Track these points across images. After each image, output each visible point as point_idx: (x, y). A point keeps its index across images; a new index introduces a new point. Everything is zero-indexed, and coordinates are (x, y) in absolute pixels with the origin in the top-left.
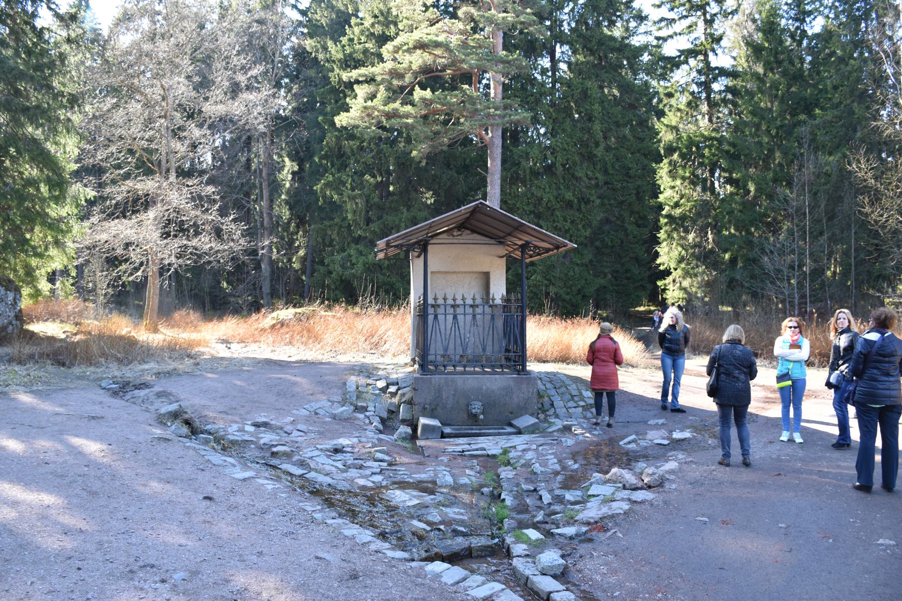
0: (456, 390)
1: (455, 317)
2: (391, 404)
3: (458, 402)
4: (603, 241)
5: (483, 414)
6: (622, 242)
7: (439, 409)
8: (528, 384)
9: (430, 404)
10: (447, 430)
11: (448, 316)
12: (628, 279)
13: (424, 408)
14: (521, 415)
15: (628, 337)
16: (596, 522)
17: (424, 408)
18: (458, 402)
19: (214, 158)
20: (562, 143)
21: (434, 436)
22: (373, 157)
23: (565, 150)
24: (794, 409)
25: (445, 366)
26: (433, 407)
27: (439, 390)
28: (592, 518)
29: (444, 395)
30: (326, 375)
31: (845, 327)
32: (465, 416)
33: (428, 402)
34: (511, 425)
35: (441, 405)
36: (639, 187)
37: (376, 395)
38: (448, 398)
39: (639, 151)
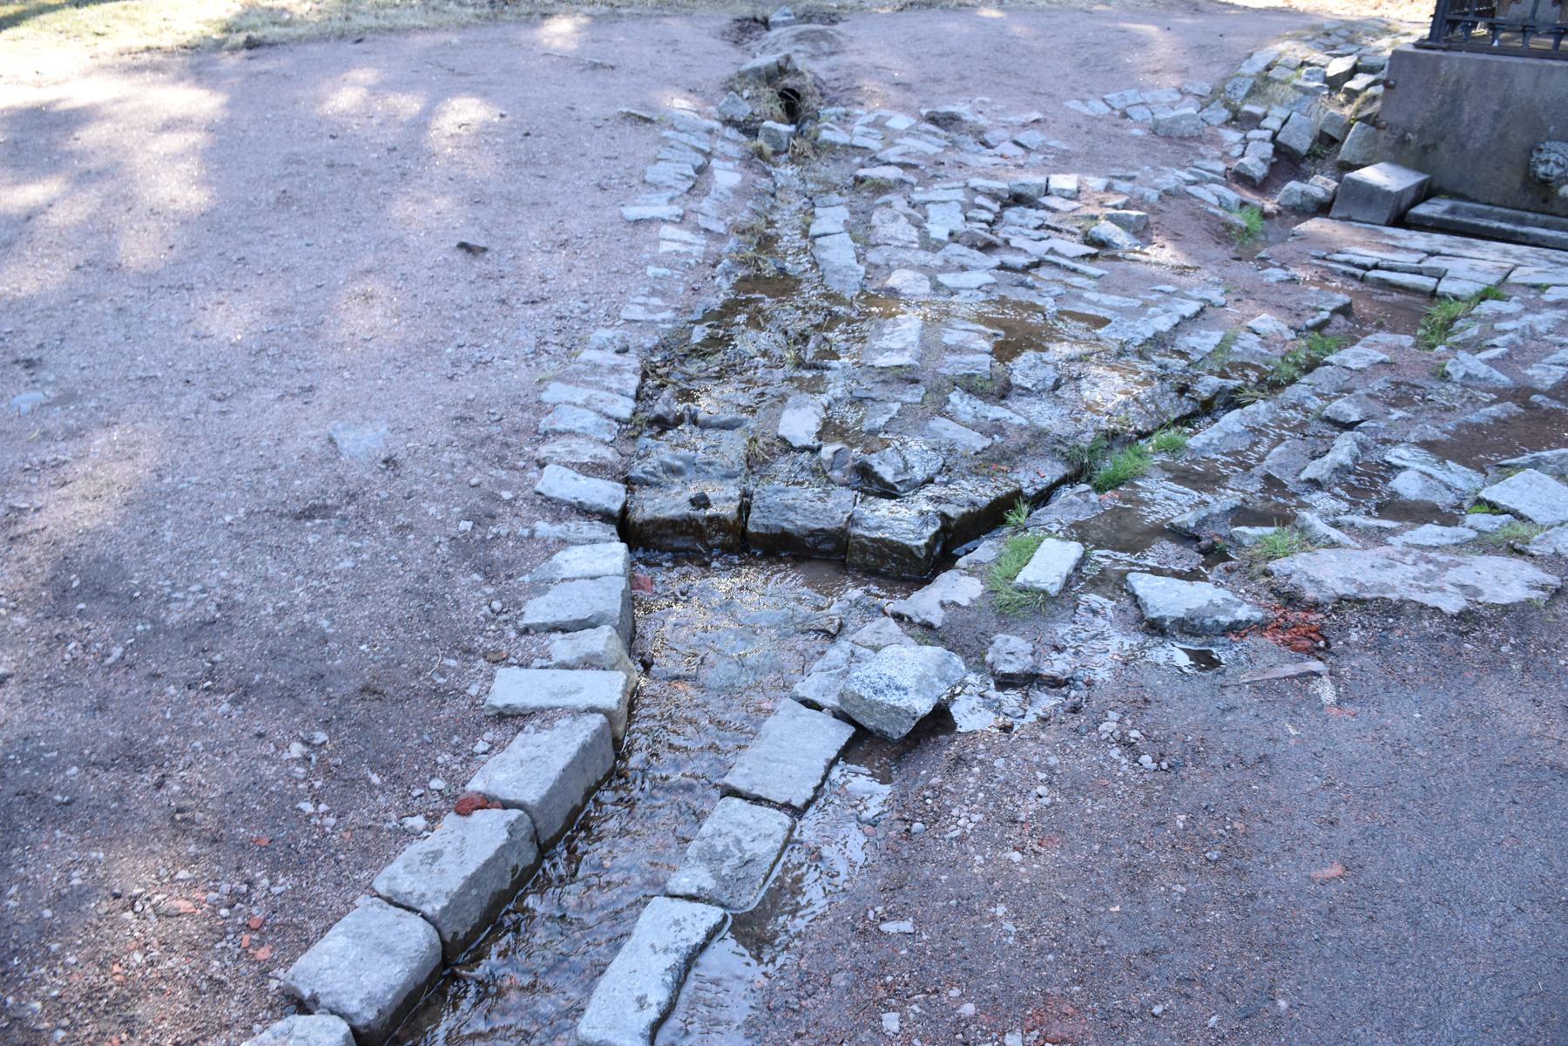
0: (1504, 103)
2: (1333, 118)
3: (1502, 137)
7: (1443, 147)
13: (1403, 141)
15: (181, 205)
16: (1316, 606)
17: (1403, 141)
18: (1502, 137)
19: (444, 194)
21: (1369, 215)
24: (1368, 529)
26: (1428, 141)
27: (1454, 98)
28: (1318, 583)
31: (428, 215)
32: (1517, 181)
33: (1417, 125)
37: (1306, 91)
38: (1476, 120)
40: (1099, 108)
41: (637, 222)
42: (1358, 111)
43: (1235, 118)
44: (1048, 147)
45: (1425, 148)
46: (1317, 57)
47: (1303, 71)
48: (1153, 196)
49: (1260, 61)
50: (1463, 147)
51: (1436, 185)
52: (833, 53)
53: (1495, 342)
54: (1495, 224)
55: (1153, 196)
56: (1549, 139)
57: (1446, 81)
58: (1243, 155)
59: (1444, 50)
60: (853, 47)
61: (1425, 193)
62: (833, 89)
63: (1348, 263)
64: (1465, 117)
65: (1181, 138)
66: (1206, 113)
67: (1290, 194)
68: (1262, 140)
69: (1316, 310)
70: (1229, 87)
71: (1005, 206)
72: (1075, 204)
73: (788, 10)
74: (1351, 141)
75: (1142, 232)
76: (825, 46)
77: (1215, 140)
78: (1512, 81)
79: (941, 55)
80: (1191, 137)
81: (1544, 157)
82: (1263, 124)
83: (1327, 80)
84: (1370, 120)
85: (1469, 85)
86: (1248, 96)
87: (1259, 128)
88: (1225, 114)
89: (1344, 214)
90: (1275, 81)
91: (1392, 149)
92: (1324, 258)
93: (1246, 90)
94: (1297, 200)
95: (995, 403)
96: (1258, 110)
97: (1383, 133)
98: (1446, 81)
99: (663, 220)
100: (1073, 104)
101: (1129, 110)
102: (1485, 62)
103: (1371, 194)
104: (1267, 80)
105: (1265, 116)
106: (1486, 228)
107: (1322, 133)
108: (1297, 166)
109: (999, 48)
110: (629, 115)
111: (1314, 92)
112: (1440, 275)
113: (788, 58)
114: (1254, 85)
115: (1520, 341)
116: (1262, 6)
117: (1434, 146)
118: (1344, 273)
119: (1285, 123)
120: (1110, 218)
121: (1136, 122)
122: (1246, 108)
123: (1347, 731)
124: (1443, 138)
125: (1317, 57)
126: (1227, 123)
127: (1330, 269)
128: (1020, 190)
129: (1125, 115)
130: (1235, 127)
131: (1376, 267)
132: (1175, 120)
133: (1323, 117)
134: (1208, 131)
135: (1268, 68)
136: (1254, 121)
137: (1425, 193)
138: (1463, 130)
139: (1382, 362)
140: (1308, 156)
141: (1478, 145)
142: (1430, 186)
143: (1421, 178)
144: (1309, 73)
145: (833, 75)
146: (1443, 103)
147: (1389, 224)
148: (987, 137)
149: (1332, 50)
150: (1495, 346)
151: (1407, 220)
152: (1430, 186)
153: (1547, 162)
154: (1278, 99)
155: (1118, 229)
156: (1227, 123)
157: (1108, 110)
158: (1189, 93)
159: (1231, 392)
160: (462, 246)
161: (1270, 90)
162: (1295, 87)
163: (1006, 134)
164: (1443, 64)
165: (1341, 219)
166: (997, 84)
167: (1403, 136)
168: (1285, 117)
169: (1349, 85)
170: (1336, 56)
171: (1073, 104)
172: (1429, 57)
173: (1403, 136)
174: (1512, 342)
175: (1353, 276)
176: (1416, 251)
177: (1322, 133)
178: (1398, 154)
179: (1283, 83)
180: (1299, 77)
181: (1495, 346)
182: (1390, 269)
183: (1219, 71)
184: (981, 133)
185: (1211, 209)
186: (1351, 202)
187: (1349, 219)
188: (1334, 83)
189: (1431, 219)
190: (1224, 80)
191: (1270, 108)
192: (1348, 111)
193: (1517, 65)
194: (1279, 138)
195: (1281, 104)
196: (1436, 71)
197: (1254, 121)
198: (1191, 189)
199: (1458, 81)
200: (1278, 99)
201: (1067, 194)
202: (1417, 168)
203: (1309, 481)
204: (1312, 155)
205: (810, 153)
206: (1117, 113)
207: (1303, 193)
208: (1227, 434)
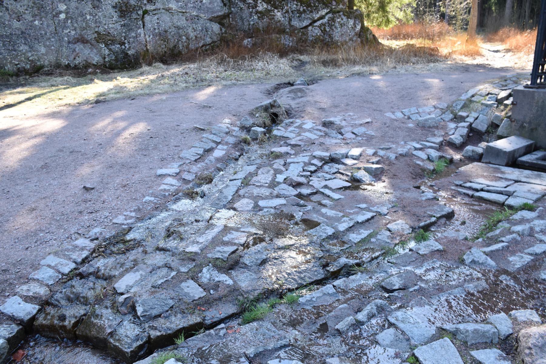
2: (497, 117)
7: (540, 129)
13: (522, 127)
17: (522, 127)
26: (533, 126)
33: (527, 120)
37: (487, 106)
40: (399, 115)
41: (160, 176)
42: (507, 113)
43: (455, 118)
44: (366, 134)
45: (532, 130)
46: (496, 91)
47: (487, 98)
48: (393, 156)
49: (471, 92)
51: (538, 145)
52: (302, 97)
53: (503, 239)
55: (393, 156)
57: (538, 101)
58: (453, 134)
59: (537, 88)
60: (311, 94)
61: (528, 150)
62: (296, 111)
63: (470, 188)
65: (429, 127)
66: (443, 116)
67: (467, 152)
68: (464, 127)
69: (432, 216)
70: (454, 105)
71: (326, 163)
72: (355, 162)
73: (302, 79)
74: (503, 126)
75: (377, 175)
76: (299, 94)
77: (444, 128)
79: (343, 96)
80: (434, 127)
82: (466, 120)
83: (497, 100)
84: (509, 117)
86: (461, 108)
87: (465, 122)
88: (451, 116)
89: (488, 161)
90: (474, 102)
91: (518, 130)
92: (461, 186)
93: (461, 106)
94: (470, 154)
95: (224, 272)
96: (464, 114)
97: (514, 124)
98: (538, 101)
99: (169, 175)
100: (389, 115)
101: (411, 116)
103: (498, 152)
104: (471, 101)
105: (468, 116)
107: (492, 122)
108: (481, 137)
109: (369, 92)
110: (196, 128)
111: (490, 106)
112: (509, 195)
113: (275, 101)
114: (465, 103)
115: (519, 238)
116: (499, 67)
117: (536, 129)
118: (464, 193)
119: (476, 119)
120: (366, 169)
121: (413, 121)
122: (460, 113)
124: (539, 126)
125: (496, 91)
126: (452, 120)
127: (459, 191)
128: (334, 156)
129: (409, 118)
130: (455, 121)
131: (482, 190)
132: (426, 120)
133: (493, 116)
134: (442, 123)
135: (473, 96)
136: (462, 119)
137: (528, 150)
139: (438, 250)
140: (486, 133)
142: (535, 146)
143: (532, 142)
144: (490, 98)
145: (297, 106)
146: (538, 111)
147: (507, 165)
148: (342, 130)
149: (503, 87)
150: (503, 242)
151: (517, 163)
152: (535, 146)
154: (475, 109)
155: (367, 174)
156: (452, 120)
157: (403, 116)
158: (438, 108)
159: (351, 266)
160: (84, 187)
161: (471, 106)
162: (482, 104)
163: (350, 129)
164: (536, 94)
165: (486, 163)
166: (360, 107)
167: (522, 125)
168: (476, 116)
169: (506, 102)
170: (503, 90)
171: (389, 115)
172: (530, 91)
173: (522, 125)
174: (514, 239)
175: (468, 195)
176: (511, 180)
177: (492, 122)
178: (520, 131)
179: (477, 102)
180: (485, 99)
181: (503, 242)
182: (488, 191)
183: (454, 98)
184: (340, 129)
185: (421, 163)
186: (493, 156)
187: (490, 163)
188: (500, 102)
189: (527, 162)
190: (453, 102)
191: (471, 113)
192: (503, 113)
194: (473, 126)
195: (476, 111)
196: (533, 98)
197: (462, 119)
198: (415, 153)
200: (475, 109)
201: (354, 157)
202: (530, 138)
203: (338, 330)
204: (487, 132)
206: (406, 117)
207: (473, 151)
208: (325, 294)
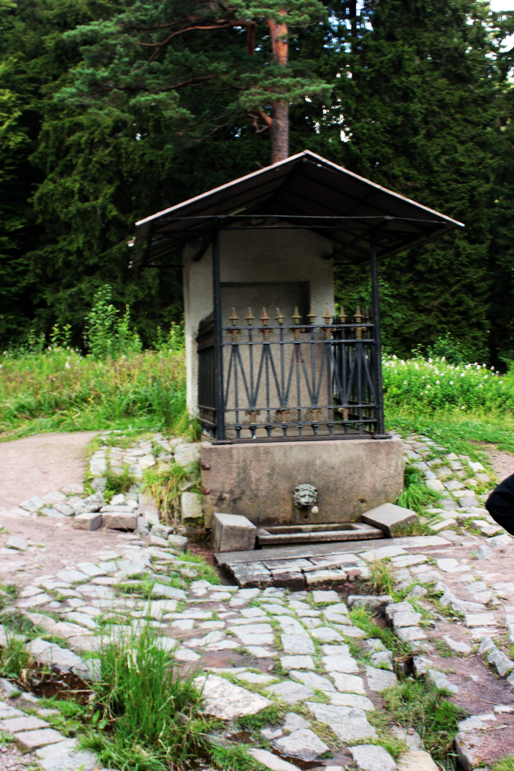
0: (273, 469)
1: (266, 348)
3: (275, 487)
4: (425, 263)
5: (316, 504)
6: (452, 264)
8: (388, 454)
9: (231, 492)
10: (265, 534)
11: (254, 348)
12: (459, 313)
13: (221, 499)
14: (379, 504)
17: (221, 499)
20: (368, 129)
22: (109, 154)
23: (373, 138)
25: (253, 429)
26: (236, 495)
27: (245, 470)
29: (254, 475)
30: (245, 671)
33: (227, 488)
34: (364, 520)
35: (248, 493)
36: (474, 188)
39: (472, 139)
45: (235, 501)
50: (256, 496)
54: (306, 535)
56: (300, 483)
64: (253, 479)
78: (273, 456)
81: (302, 493)
85: (251, 461)
97: (208, 497)
102: (257, 448)
106: (309, 538)
123: (174, 733)
138: (253, 486)
141: (264, 493)
146: (239, 474)
153: (304, 496)
164: (234, 451)
167: (221, 496)
172: (225, 449)
173: (221, 496)
193: (273, 447)
196: (231, 456)
199: (244, 460)
205: (422, 622)
